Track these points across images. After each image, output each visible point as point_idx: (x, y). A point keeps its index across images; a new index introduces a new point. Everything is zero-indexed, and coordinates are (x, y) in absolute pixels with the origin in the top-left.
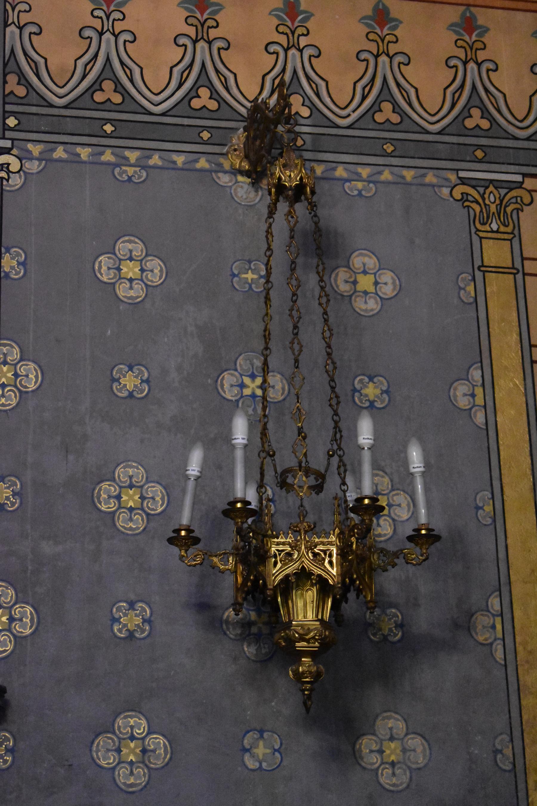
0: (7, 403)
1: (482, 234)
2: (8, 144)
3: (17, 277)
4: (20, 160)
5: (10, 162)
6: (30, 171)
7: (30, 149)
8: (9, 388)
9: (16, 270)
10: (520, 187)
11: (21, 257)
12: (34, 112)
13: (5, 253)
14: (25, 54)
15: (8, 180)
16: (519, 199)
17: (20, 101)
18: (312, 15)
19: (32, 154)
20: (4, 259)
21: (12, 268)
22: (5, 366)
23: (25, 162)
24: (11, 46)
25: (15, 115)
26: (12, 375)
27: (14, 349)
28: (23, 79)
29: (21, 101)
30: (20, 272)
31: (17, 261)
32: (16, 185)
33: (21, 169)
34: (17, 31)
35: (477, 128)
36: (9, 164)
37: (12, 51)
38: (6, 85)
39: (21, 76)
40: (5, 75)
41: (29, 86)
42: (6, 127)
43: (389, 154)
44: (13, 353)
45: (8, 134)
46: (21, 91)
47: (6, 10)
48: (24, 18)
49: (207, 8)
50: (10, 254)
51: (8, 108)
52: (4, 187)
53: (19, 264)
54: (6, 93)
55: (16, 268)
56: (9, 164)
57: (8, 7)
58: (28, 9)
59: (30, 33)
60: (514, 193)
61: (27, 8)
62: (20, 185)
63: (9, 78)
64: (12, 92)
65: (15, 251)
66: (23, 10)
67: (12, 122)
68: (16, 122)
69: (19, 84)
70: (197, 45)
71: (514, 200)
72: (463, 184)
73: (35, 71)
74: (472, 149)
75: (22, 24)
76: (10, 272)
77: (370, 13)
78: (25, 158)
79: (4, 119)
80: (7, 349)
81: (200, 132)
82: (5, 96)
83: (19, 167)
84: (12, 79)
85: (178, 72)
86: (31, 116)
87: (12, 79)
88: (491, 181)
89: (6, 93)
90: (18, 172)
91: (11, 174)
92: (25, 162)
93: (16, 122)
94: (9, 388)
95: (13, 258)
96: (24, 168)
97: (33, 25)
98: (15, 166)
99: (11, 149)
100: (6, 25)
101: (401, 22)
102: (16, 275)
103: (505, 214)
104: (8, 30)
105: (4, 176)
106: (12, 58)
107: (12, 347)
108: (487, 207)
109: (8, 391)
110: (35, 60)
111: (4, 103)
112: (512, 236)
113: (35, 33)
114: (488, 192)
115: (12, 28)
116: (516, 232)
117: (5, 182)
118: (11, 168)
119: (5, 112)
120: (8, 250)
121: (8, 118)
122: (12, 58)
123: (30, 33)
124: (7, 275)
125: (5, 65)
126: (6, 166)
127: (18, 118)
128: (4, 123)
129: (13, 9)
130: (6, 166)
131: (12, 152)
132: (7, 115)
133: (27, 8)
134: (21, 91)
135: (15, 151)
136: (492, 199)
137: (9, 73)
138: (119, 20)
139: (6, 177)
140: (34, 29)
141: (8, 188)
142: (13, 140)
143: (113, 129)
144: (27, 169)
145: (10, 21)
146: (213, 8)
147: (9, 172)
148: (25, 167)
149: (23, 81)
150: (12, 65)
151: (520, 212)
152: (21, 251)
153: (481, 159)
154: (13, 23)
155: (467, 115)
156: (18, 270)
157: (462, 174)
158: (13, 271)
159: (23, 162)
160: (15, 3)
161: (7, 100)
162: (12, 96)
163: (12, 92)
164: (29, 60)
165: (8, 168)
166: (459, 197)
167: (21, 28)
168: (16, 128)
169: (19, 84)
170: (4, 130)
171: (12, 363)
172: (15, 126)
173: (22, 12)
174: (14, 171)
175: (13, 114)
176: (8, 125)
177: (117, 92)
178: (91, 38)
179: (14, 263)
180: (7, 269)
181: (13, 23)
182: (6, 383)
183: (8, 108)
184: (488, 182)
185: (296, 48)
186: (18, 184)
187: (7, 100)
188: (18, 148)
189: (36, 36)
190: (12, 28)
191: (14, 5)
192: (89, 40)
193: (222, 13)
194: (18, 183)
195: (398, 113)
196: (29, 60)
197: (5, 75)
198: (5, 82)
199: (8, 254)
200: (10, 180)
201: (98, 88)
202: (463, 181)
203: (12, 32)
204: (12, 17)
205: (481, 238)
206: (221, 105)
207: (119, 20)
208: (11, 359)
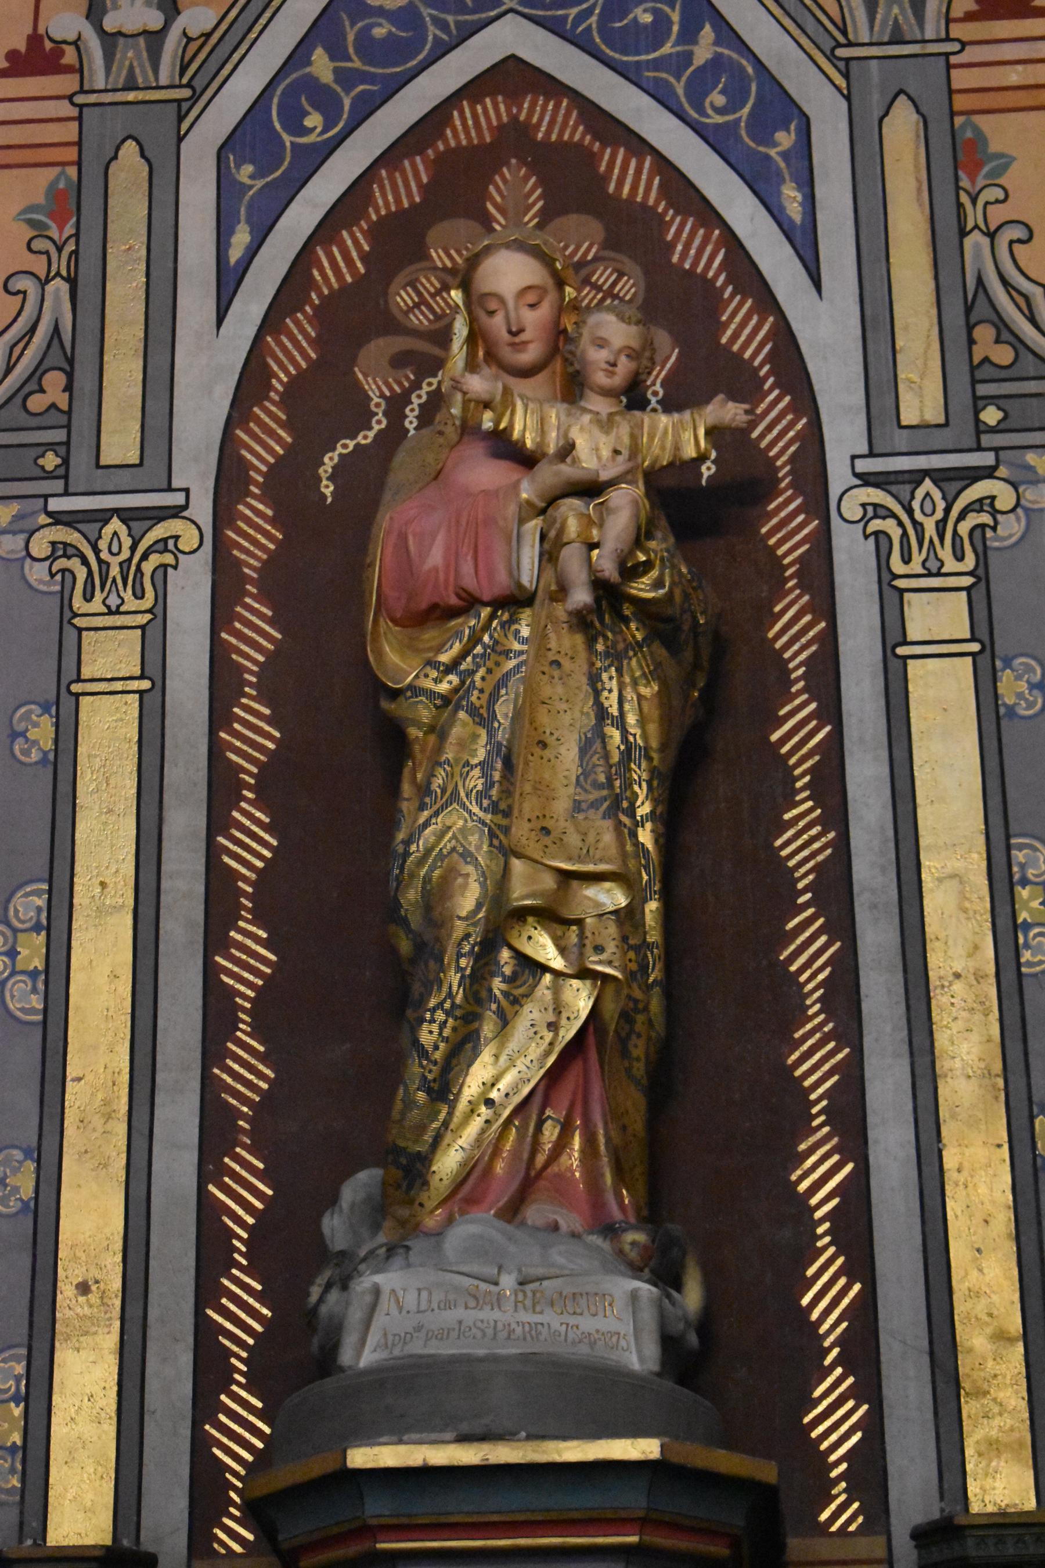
0: (1036, 960)
1: (901, 583)
2: (987, 459)
3: (1031, 712)
4: (1015, 486)
5: (995, 493)
6: (1036, 506)
7: (1032, 463)
8: (1036, 930)
9: (1026, 700)
10: (991, 476)
11: (1035, 672)
12: (1034, 391)
13: (1003, 670)
14: (1005, 282)
15: (994, 529)
16: (171, 542)
17: (1004, 374)
18: (1014, 159)
19: (1036, 472)
20: (1001, 682)
21: (1020, 696)
22: (1024, 888)
23: (1025, 490)
24: (976, 271)
25: (996, 401)
26: (1041, 904)
27: (1038, 854)
28: (1004, 331)
29: (1007, 374)
30: (1035, 703)
31: (1028, 682)
32: (1011, 536)
33: (1018, 504)
34: (986, 241)
35: (53, 411)
36: (993, 498)
37: (980, 282)
38: (975, 347)
39: (1002, 327)
40: (970, 328)
41: (1018, 342)
42: (982, 427)
43: (48, 472)
44: (1038, 860)
45: (986, 440)
46: (1003, 355)
47: (960, 205)
48: (997, 215)
49: (980, 165)
50: (1013, 670)
51: (982, 390)
52: (988, 543)
53: (1032, 686)
54: (976, 361)
55: (1028, 696)
56: (993, 498)
57: (964, 198)
58: (1002, 196)
59: (1011, 242)
60: (159, 531)
61: (1001, 195)
62: (1019, 535)
63: (979, 332)
64: (986, 360)
65: (1021, 664)
66: (992, 200)
67: (991, 416)
68: (1000, 415)
69: (997, 341)
70: (48, 288)
71: (160, 546)
72: (57, 523)
73: (1026, 312)
74: (33, 452)
75: (992, 228)
76: (1015, 704)
77: (40, 199)
78: (1024, 483)
79: (977, 412)
80: (1025, 856)
81: (38, 457)
82: (973, 369)
83: (1013, 502)
84: (984, 334)
85: (1034, 294)
86: (1028, 400)
87: (984, 334)
88: (926, 473)
89: (976, 361)
90: (1013, 510)
91: (999, 517)
92: (1025, 490)
93: (1000, 415)
94: (1036, 930)
95: (1019, 678)
96: (1023, 502)
97: (1013, 225)
98: (1005, 498)
99: (995, 468)
100: (963, 233)
101: (1014, 159)
102: (1028, 708)
103: (139, 575)
104: (968, 242)
105: (167, 562)
106: (981, 295)
107: (1036, 849)
108: (104, 567)
109: (1036, 936)
110: (1024, 291)
111: (974, 382)
112: (149, 616)
113: (1020, 241)
114: (920, 493)
115: (977, 235)
116: (159, 610)
117: (989, 533)
118: (999, 505)
119: (976, 398)
120: (1008, 663)
121: (984, 408)
122: (981, 295)
123: (1011, 242)
124: (1011, 710)
125: (968, 310)
126: (988, 501)
127: (1002, 406)
128: (977, 421)
129: (974, 201)
130: (988, 501)
131: (997, 474)
132: (981, 403)
133: (1001, 195)
134: (1003, 355)
135: (1002, 471)
136: (928, 509)
137: (976, 324)
138: (997, 201)
139: (992, 523)
140: (1018, 233)
141: (996, 544)
142: (996, 450)
143: (41, 461)
144: (1030, 502)
145: (970, 225)
146: (994, 164)
147: (994, 512)
148: (1026, 500)
149: (1005, 335)
150: (981, 308)
151: (170, 570)
152: (1033, 663)
153: (52, 472)
154: (976, 227)
155: (36, 387)
156: (1031, 699)
157: (54, 505)
158: (1022, 702)
159: (1021, 490)
160: (978, 189)
161: (979, 375)
162: (987, 365)
163: (986, 360)
164: (1014, 293)
165: (992, 505)
166: (858, 514)
167: (992, 235)
168: (1002, 426)
169: (997, 341)
170: (978, 433)
171: (1038, 880)
172: (999, 422)
173: (992, 203)
174: (1004, 509)
175: (991, 399)
176: (984, 423)
177: (1003, 342)
178: (25, 293)
179: (1023, 686)
180: (1010, 700)
181: (976, 227)
182: (1029, 920)
183: (982, 390)
184: (922, 474)
185: (63, 278)
186: (1014, 535)
187: (979, 375)
188: (1011, 464)
189: (1021, 246)
190: (977, 235)
191: (974, 192)
192: (21, 296)
193: (1014, 169)
194: (1014, 531)
195: (1006, 342)
196: (1014, 293)
197: (970, 328)
198: (971, 342)
199: (1008, 671)
200: (999, 527)
201: (36, 387)
202: (59, 519)
203: (977, 246)
204: (973, 216)
205: (80, 630)
206: (1021, 355)
207: (997, 201)
208: (1034, 872)
